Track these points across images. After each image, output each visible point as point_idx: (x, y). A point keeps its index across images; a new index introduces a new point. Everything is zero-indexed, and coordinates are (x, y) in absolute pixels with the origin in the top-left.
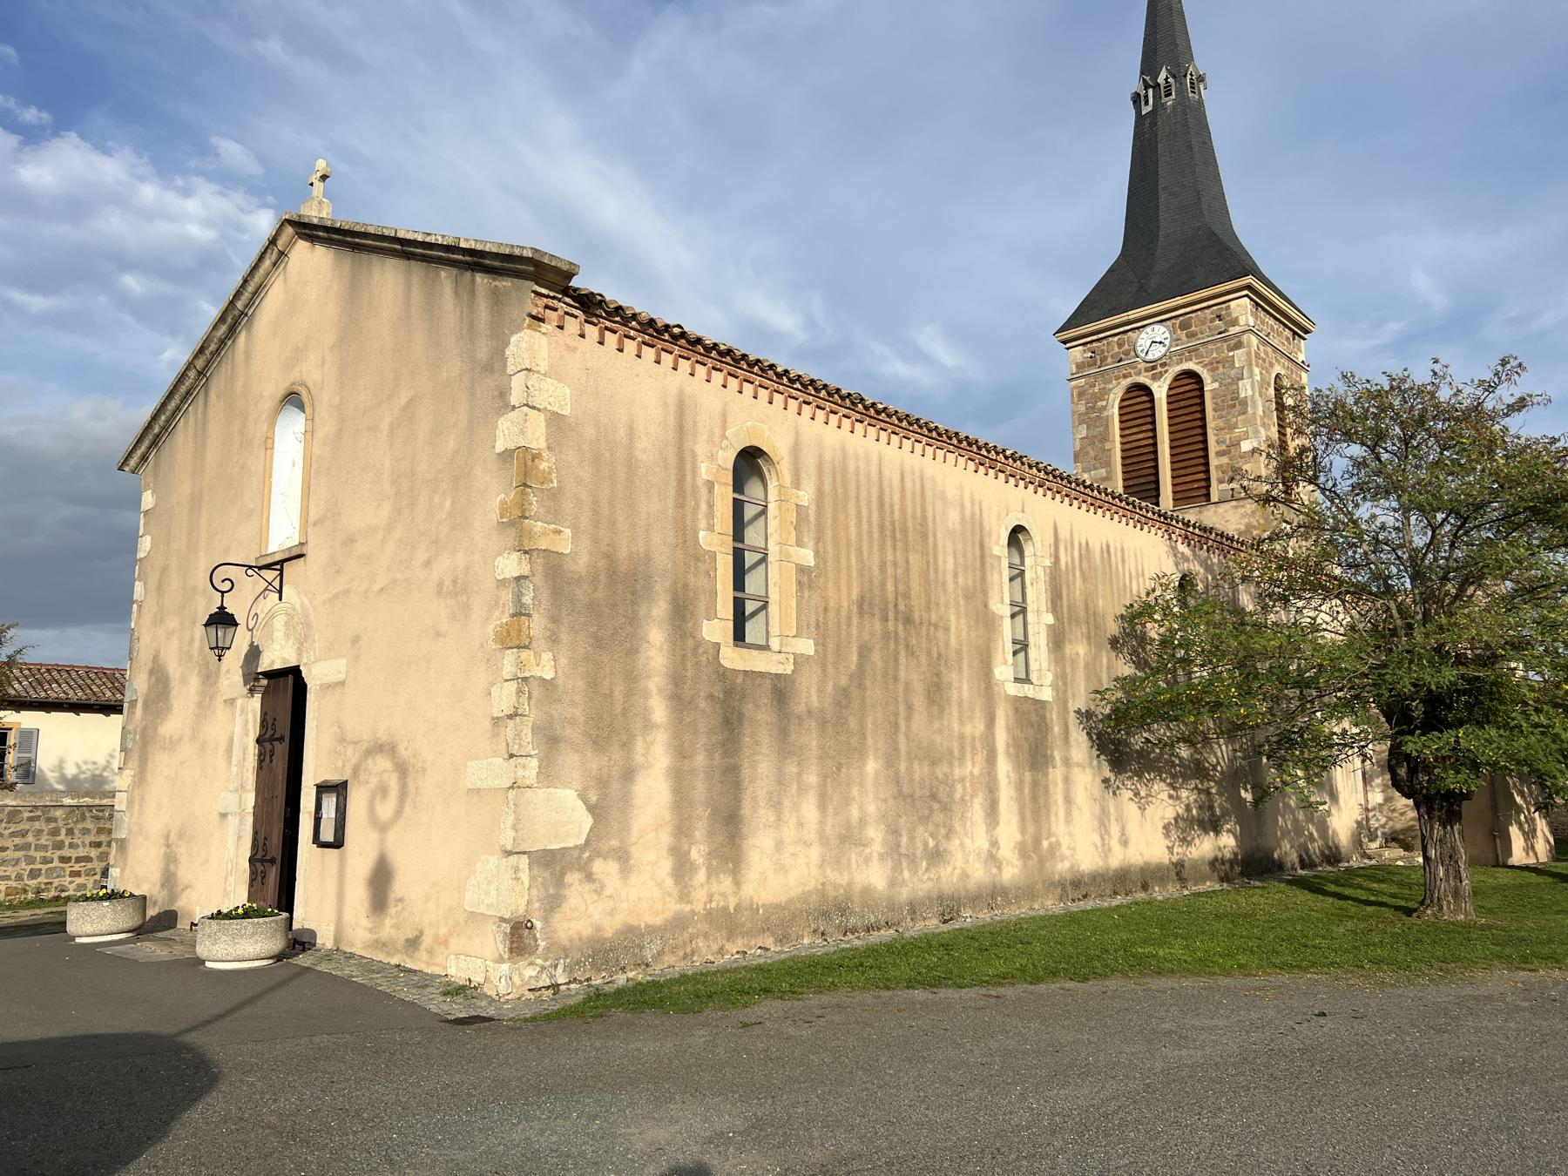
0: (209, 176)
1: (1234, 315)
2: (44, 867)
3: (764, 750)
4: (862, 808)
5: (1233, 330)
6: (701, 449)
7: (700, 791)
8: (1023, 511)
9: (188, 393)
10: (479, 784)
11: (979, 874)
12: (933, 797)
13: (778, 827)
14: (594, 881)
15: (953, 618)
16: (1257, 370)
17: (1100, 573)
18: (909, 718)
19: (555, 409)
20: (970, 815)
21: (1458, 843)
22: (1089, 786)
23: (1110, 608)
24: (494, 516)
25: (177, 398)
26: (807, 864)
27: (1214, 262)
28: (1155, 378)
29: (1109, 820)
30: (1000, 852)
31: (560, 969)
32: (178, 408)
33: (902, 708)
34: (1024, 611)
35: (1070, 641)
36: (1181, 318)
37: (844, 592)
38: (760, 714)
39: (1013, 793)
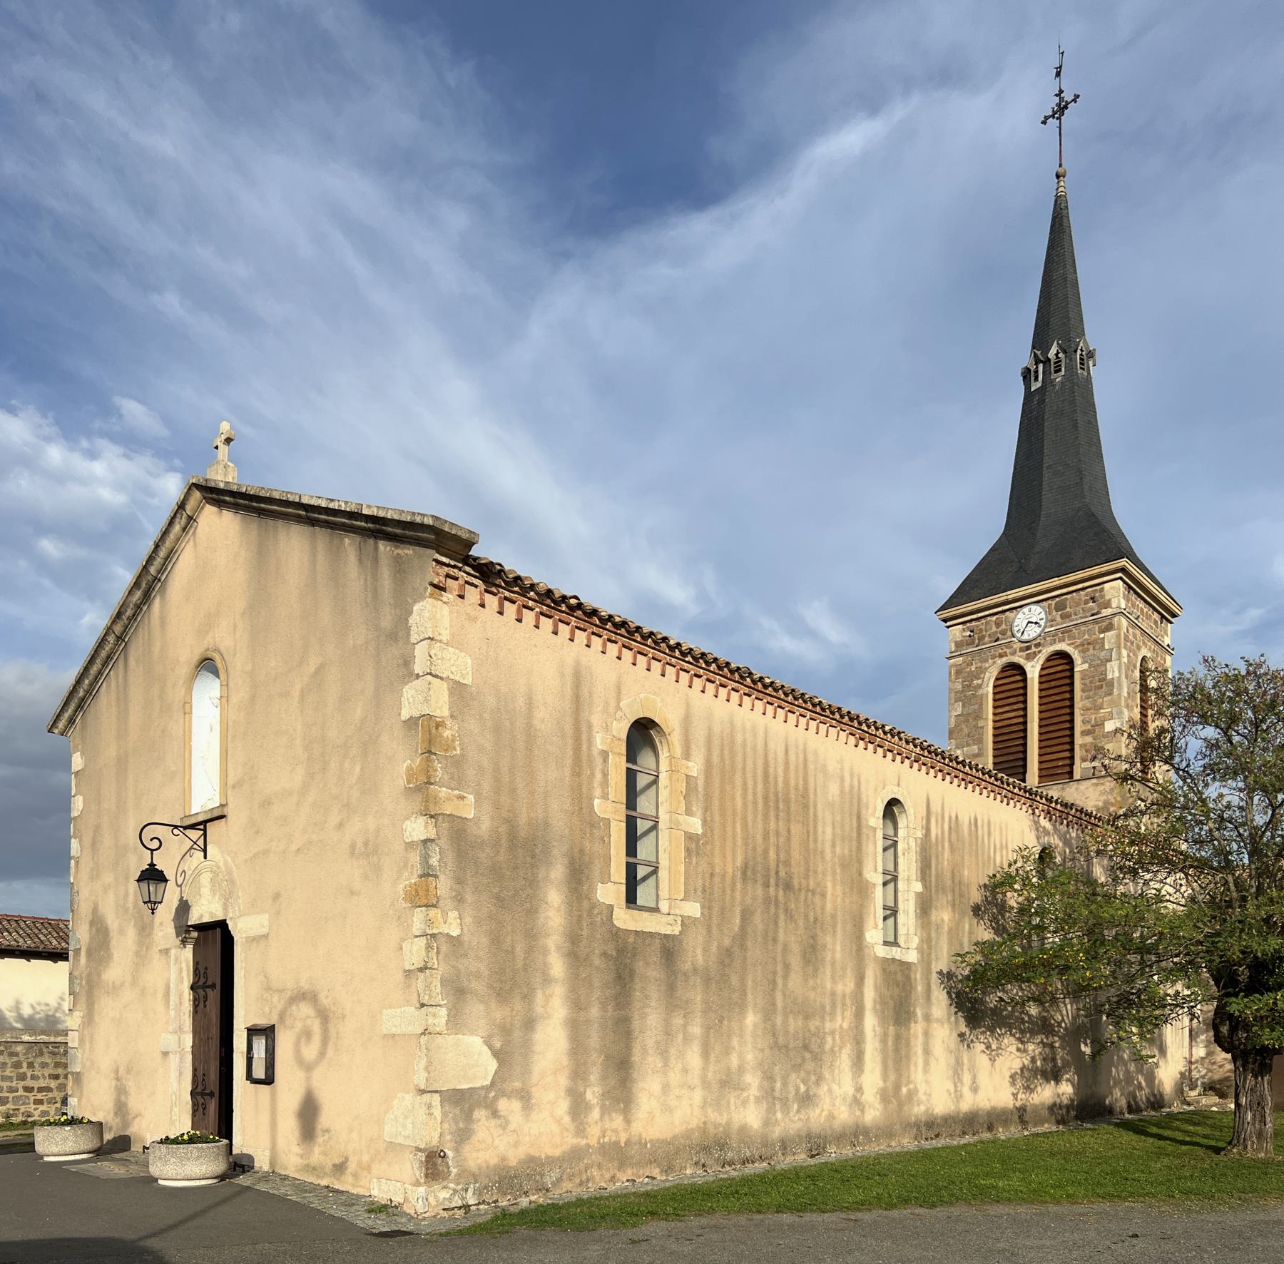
0: (115, 438)
1: (1107, 598)
2: (11, 1095)
3: (653, 1004)
4: (740, 1056)
5: (1105, 612)
6: (596, 720)
7: (594, 1039)
8: (899, 785)
9: (109, 658)
10: (394, 1030)
11: (844, 1116)
12: (806, 1047)
13: (665, 1073)
14: (499, 1117)
15: (829, 885)
16: (1124, 653)
17: (967, 845)
18: (786, 977)
19: (457, 678)
20: (838, 1064)
21: (1267, 1092)
22: (946, 1039)
23: (975, 878)
24: (401, 782)
25: (98, 663)
26: (691, 1105)
27: (1092, 543)
28: (1029, 658)
29: (962, 1070)
30: (864, 1096)
31: (470, 1192)
32: (100, 673)
33: (780, 967)
34: (895, 879)
35: (936, 909)
36: (1057, 599)
37: (729, 859)
38: (650, 971)
39: (877, 1044)
